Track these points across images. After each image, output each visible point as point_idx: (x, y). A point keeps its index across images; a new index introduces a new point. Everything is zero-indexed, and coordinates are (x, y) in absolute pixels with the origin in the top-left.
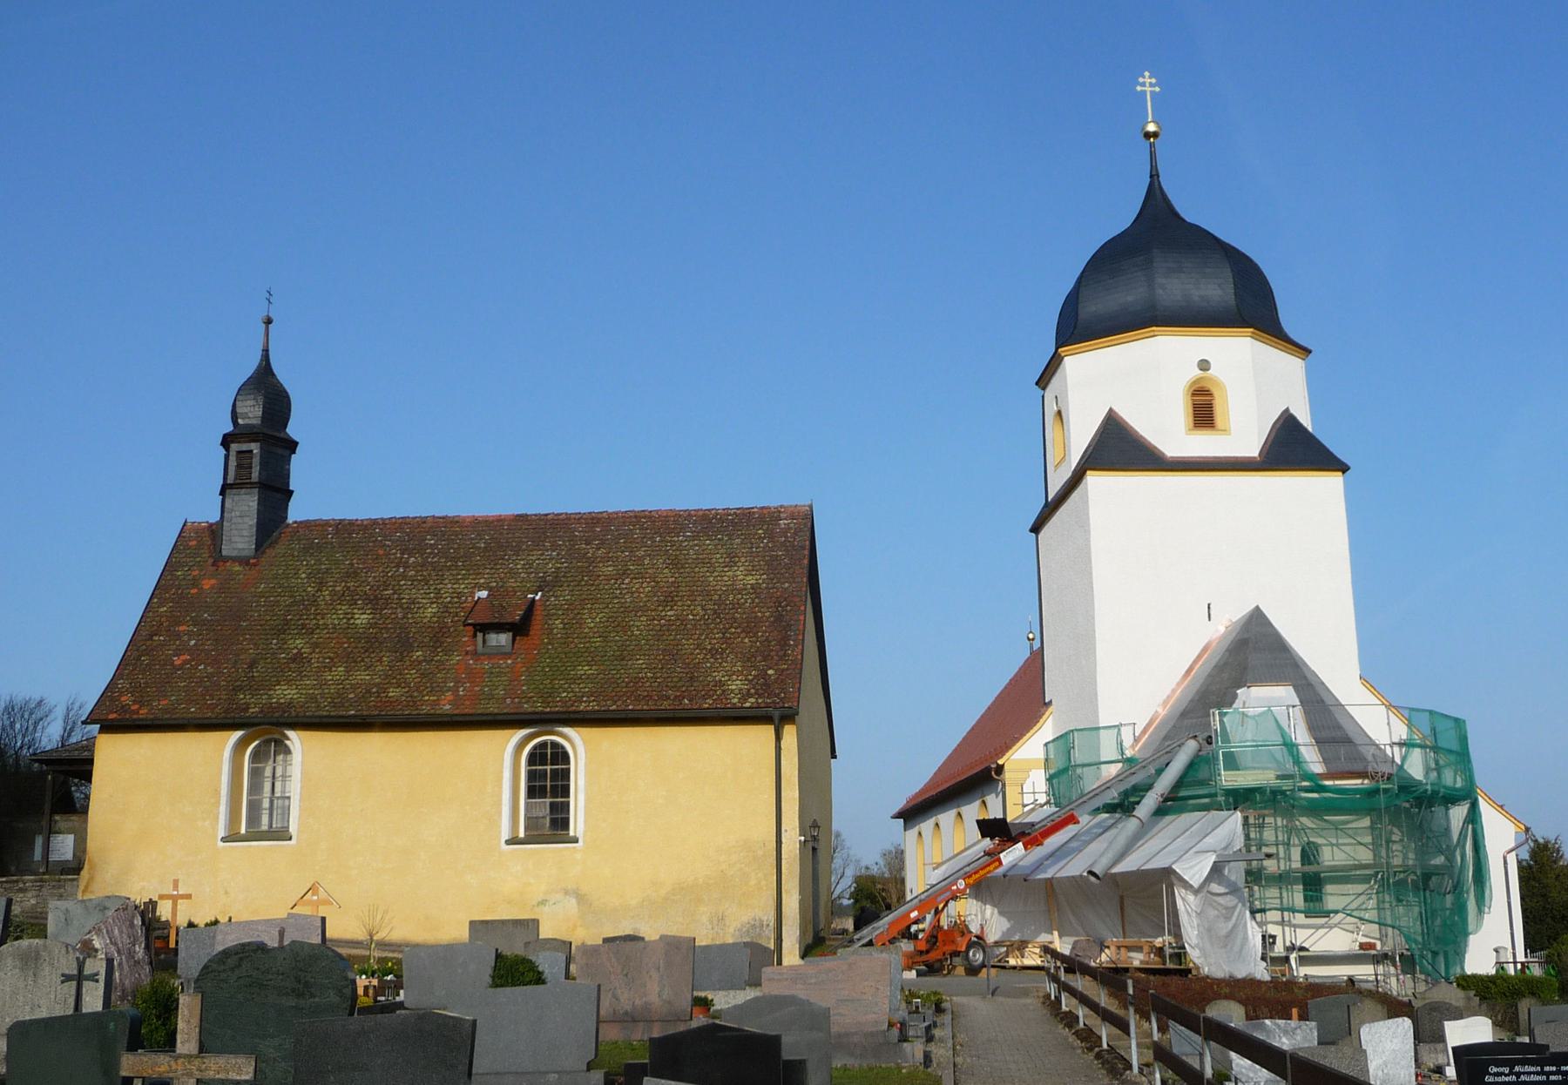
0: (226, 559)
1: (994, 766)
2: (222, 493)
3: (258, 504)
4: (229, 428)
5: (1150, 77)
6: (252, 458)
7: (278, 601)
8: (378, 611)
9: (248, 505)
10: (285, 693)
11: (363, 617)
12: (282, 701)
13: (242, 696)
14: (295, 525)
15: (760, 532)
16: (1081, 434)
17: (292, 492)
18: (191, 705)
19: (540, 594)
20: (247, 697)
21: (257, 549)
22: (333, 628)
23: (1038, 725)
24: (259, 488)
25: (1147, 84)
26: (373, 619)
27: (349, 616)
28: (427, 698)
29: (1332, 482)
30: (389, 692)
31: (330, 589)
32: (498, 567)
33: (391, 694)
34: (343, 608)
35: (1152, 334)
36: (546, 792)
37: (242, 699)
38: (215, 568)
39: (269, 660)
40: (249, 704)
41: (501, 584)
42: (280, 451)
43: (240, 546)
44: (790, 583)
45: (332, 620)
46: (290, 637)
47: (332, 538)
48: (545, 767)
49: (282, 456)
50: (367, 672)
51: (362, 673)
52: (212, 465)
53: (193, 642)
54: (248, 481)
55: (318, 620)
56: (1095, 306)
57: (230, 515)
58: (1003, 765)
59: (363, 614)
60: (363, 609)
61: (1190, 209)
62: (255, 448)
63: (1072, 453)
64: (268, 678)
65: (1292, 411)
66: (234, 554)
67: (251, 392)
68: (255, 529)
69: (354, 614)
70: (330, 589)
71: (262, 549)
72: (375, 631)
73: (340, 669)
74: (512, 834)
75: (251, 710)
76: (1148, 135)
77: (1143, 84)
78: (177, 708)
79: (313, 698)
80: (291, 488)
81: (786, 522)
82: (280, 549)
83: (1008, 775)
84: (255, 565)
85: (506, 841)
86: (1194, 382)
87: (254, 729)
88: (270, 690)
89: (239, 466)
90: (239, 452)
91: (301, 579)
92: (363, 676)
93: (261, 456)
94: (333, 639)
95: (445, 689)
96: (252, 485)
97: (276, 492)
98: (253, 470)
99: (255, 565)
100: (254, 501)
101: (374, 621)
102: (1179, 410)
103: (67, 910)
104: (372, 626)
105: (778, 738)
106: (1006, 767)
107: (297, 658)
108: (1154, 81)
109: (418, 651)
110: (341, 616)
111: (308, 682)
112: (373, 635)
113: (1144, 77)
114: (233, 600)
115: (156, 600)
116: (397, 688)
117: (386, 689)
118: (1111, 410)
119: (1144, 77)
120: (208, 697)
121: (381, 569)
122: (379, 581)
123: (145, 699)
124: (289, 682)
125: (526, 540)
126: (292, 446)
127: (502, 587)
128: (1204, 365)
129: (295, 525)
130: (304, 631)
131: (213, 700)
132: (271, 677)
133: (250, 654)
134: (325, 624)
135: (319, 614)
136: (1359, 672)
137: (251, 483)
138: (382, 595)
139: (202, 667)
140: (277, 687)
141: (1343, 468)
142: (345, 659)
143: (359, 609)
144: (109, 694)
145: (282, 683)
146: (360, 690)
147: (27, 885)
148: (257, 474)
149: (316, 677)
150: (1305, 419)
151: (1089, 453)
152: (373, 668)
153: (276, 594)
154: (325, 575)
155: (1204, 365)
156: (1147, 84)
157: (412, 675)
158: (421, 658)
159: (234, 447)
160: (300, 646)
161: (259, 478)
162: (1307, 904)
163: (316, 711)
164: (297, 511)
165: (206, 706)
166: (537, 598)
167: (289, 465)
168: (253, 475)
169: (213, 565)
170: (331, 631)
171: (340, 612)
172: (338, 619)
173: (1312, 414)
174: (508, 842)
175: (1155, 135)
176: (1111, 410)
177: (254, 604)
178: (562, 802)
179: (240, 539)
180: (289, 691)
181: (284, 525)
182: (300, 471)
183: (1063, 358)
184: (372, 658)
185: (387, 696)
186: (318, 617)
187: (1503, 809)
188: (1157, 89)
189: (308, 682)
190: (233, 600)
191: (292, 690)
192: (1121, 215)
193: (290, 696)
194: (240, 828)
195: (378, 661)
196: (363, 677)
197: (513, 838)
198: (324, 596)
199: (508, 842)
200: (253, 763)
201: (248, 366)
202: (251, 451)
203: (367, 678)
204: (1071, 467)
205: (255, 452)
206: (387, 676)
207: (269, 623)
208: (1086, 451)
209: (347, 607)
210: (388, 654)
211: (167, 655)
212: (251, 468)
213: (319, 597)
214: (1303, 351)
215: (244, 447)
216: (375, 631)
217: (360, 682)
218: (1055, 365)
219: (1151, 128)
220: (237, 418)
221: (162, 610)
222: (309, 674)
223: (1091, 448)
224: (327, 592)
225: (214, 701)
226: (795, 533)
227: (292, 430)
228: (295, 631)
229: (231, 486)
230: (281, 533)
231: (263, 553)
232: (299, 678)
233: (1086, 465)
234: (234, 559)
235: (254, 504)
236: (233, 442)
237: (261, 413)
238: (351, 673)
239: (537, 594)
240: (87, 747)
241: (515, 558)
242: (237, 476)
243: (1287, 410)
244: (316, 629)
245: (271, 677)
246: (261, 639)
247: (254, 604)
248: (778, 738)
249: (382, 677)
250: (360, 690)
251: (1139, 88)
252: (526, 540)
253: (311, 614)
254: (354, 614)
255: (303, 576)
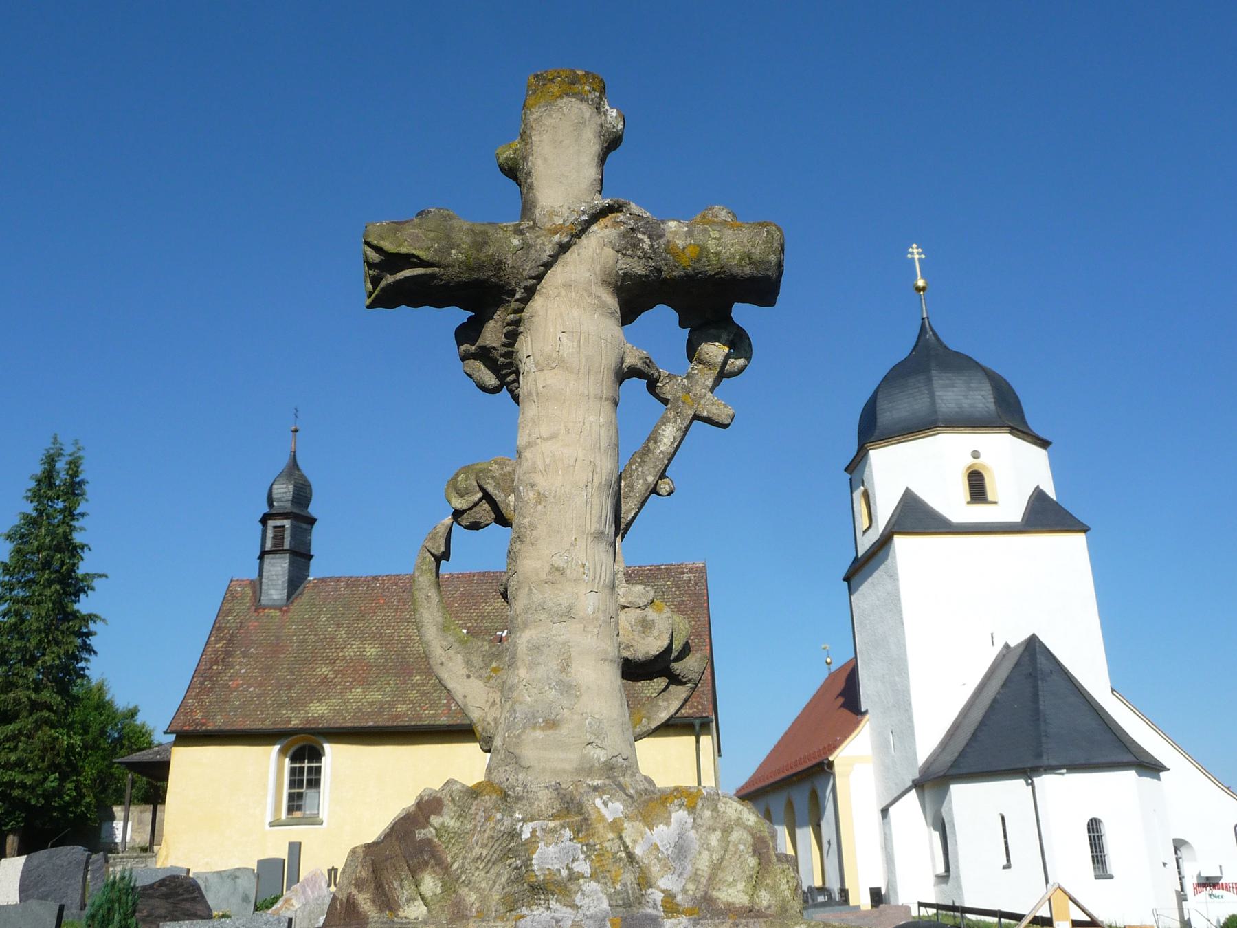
0: (265, 607)
1: (826, 762)
2: (261, 558)
3: (289, 565)
4: (266, 510)
5: (917, 248)
6: (284, 531)
7: (307, 639)
8: (384, 645)
9: (279, 568)
10: (318, 708)
11: (372, 650)
12: (316, 715)
13: (284, 712)
14: (316, 581)
15: (669, 583)
16: (885, 509)
17: (312, 556)
18: (246, 720)
19: (506, 631)
20: (289, 712)
21: (289, 596)
22: (350, 659)
23: (858, 730)
24: (290, 553)
25: (915, 253)
26: (380, 651)
27: (362, 650)
28: (427, 712)
29: (1079, 540)
30: (397, 708)
31: (346, 629)
32: (472, 611)
33: (398, 710)
34: (357, 643)
35: (936, 432)
36: (298, 782)
37: (285, 714)
38: (256, 614)
39: (303, 684)
40: (291, 717)
41: (475, 624)
42: (305, 526)
43: (275, 597)
44: (696, 621)
45: (349, 653)
46: (317, 666)
47: (344, 591)
48: (309, 765)
49: (306, 529)
50: (379, 693)
51: (376, 693)
52: (251, 537)
53: (243, 671)
54: (281, 548)
55: (339, 653)
56: (891, 412)
57: (267, 574)
58: (833, 761)
59: (372, 648)
60: (371, 644)
61: (955, 341)
62: (287, 523)
63: (879, 520)
64: (303, 698)
65: (1041, 487)
66: (270, 603)
67: (284, 482)
68: (286, 585)
69: (366, 648)
70: (346, 629)
71: (291, 600)
72: (382, 661)
73: (357, 690)
74: (275, 816)
75: (293, 723)
76: (919, 289)
77: (912, 253)
78: (235, 721)
79: (339, 712)
80: (312, 553)
81: (687, 575)
82: (305, 597)
83: (837, 769)
84: (286, 611)
85: (270, 823)
86: (969, 468)
87: (290, 739)
88: (306, 707)
89: (275, 538)
90: (275, 527)
91: (323, 621)
92: (378, 696)
93: (292, 530)
94: (350, 667)
95: (441, 705)
96: (284, 551)
97: (301, 557)
98: (285, 540)
99: (286, 611)
100: (285, 563)
101: (381, 653)
102: (962, 489)
103: (206, 878)
104: (381, 657)
105: (698, 742)
106: (835, 762)
107: (325, 681)
108: (920, 250)
109: (416, 676)
110: (356, 650)
111: (335, 701)
112: (381, 664)
113: (912, 248)
114: (272, 638)
115: (213, 639)
116: (403, 704)
117: (395, 705)
118: (907, 489)
119: (912, 248)
120: (258, 713)
121: (383, 614)
122: (382, 622)
123: (210, 714)
124: (320, 701)
125: (491, 591)
126: (312, 521)
127: (476, 626)
128: (976, 455)
129: (316, 581)
130: (328, 661)
131: (262, 714)
132: (306, 697)
133: (287, 679)
134: (343, 656)
135: (338, 648)
136: (1109, 685)
137: (283, 550)
138: (385, 634)
139: (252, 689)
140: (311, 705)
141: (1084, 529)
142: (362, 683)
143: (369, 644)
144: (183, 710)
145: (315, 701)
146: (375, 706)
147: (117, 860)
148: (288, 543)
149: (340, 697)
150: (1051, 493)
151: (894, 520)
152: (383, 689)
153: (304, 634)
154: (341, 619)
155: (976, 455)
156: (915, 253)
157: (413, 694)
158: (419, 681)
159: (271, 523)
160: (326, 673)
161: (290, 547)
162: (8, 856)
163: (343, 723)
164: (317, 570)
165: (258, 720)
166: (504, 635)
167: (310, 536)
168: (285, 544)
169: (255, 612)
170: (349, 661)
171: (354, 647)
172: (354, 652)
173: (1056, 490)
174: (272, 825)
175: (923, 289)
176: (907, 489)
177: (288, 642)
178: (294, 788)
179: (275, 591)
180: (320, 708)
181: (306, 581)
182: (319, 540)
183: (868, 450)
184: (382, 682)
185: (396, 711)
186: (339, 650)
187: (1230, 790)
188: (923, 256)
189: (335, 701)
190: (272, 638)
191: (323, 706)
192: (902, 349)
193: (322, 711)
194: (281, 815)
195: (386, 684)
196: (376, 696)
197: (274, 821)
198: (341, 634)
199: (272, 825)
200: (291, 763)
201: (283, 462)
202: (283, 526)
203: (380, 697)
204: (878, 531)
205: (287, 526)
206: (395, 695)
207: (300, 656)
208: (889, 520)
209: (359, 642)
210: (394, 679)
211: (224, 681)
212: (283, 538)
213: (337, 635)
214: (1044, 443)
215: (279, 523)
216: (382, 661)
217: (374, 700)
218: (863, 455)
219: (921, 283)
220: (272, 502)
221: (217, 646)
222: (335, 694)
223: (895, 517)
224: (343, 632)
225: (263, 716)
226: (696, 584)
227: (313, 510)
228: (322, 661)
229: (270, 552)
230: (305, 587)
231: (293, 602)
232: (327, 697)
233: (896, 529)
234: (271, 607)
235: (286, 565)
236: (270, 519)
237: (291, 498)
238: (367, 693)
239: (503, 632)
240: (159, 752)
241: (484, 604)
242: (274, 545)
243: (1038, 487)
244: (337, 659)
245: (306, 697)
246: (295, 668)
247: (288, 642)
248: (698, 742)
249: (391, 696)
250: (375, 706)
251: (909, 256)
252: (491, 591)
253: (332, 648)
254: (366, 648)
255: (324, 619)
